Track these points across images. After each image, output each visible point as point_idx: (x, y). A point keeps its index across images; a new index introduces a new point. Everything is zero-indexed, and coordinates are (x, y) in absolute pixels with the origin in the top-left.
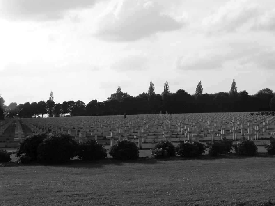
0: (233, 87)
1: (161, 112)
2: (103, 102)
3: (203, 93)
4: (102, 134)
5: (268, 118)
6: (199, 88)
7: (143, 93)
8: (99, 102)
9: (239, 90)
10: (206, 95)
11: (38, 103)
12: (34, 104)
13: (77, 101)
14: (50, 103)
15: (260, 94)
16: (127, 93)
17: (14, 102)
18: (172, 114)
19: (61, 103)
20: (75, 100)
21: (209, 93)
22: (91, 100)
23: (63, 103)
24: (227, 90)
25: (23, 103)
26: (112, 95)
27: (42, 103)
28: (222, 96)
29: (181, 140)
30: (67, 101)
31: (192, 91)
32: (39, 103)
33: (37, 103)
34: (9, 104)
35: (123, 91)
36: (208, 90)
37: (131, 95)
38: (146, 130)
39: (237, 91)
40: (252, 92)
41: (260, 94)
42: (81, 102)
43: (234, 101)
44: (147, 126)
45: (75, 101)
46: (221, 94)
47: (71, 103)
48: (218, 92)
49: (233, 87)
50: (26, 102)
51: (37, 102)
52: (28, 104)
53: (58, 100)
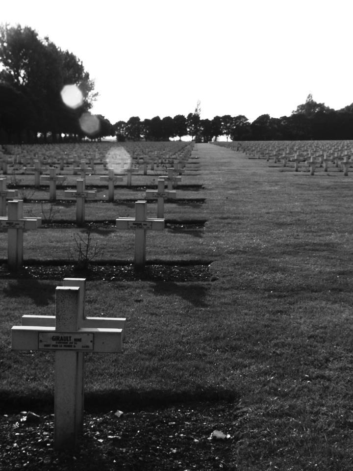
2: (281, 118)
5: (4, 385)
6: (72, 53)
8: (272, 118)
11: (271, 118)
12: (168, 119)
13: (238, 115)
14: (194, 118)
15: (78, 85)
16: (324, 104)
17: (135, 116)
19: (211, 118)
20: (234, 115)
22: (260, 115)
23: (215, 118)
25: (150, 117)
27: (180, 118)
29: (86, 235)
30: (221, 115)
32: (175, 117)
33: (171, 118)
34: (128, 119)
37: (330, 108)
39: (62, 50)
41: (78, 85)
42: (244, 117)
45: (232, 116)
47: (227, 118)
48: (223, 115)
50: (156, 116)
52: (157, 119)
53: (207, 114)
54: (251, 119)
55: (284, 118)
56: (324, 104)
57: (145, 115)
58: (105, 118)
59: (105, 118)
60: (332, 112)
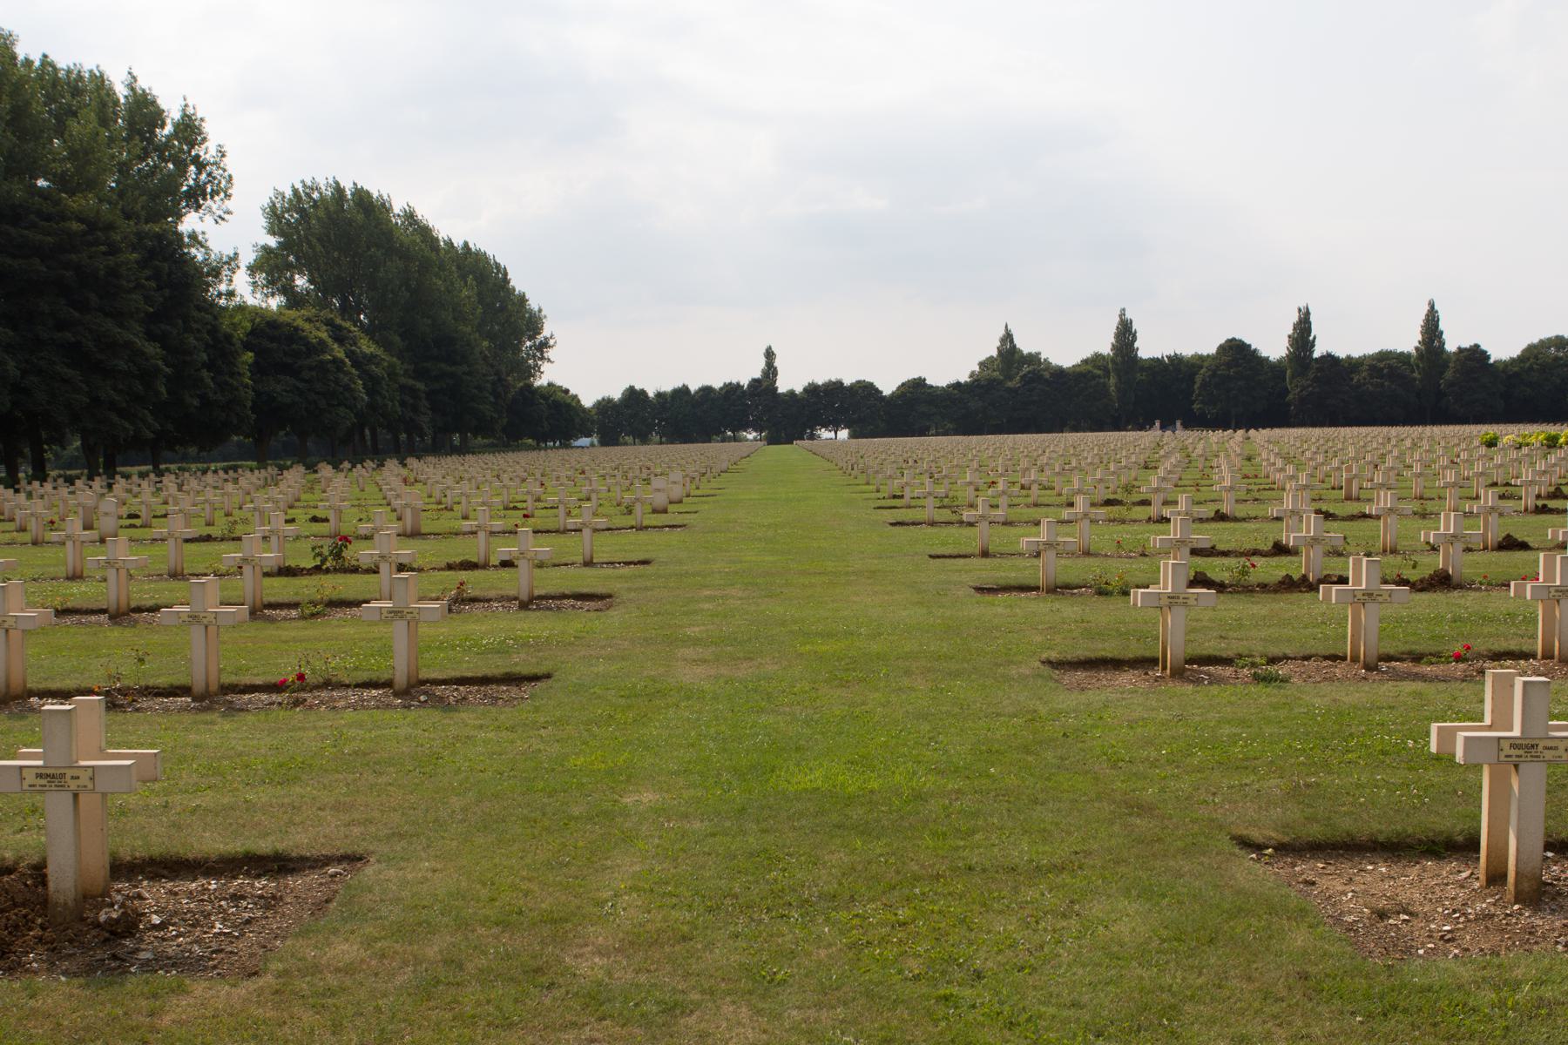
0: (1125, 333)
1: (1157, 424)
3: (1451, 347)
4: (180, 487)
7: (1477, 346)
9: (1454, 341)
10: (1329, 359)
12: (706, 391)
18: (1252, 432)
19: (799, 389)
21: (1341, 354)
22: (868, 380)
24: (1407, 341)
25: (667, 387)
26: (981, 364)
27: (732, 390)
28: (1386, 365)
30: (820, 381)
31: (1273, 346)
35: (1025, 345)
36: (1330, 341)
38: (1170, 472)
40: (1503, 348)
43: (1434, 386)
44: (1173, 460)
46: (1384, 356)
47: (835, 388)
48: (1371, 348)
49: (1125, 333)
51: (694, 387)
54: (887, 387)
55: (958, 385)
56: (1009, 352)
57: (656, 383)
58: (693, 388)
59: (693, 388)
60: (1060, 373)
